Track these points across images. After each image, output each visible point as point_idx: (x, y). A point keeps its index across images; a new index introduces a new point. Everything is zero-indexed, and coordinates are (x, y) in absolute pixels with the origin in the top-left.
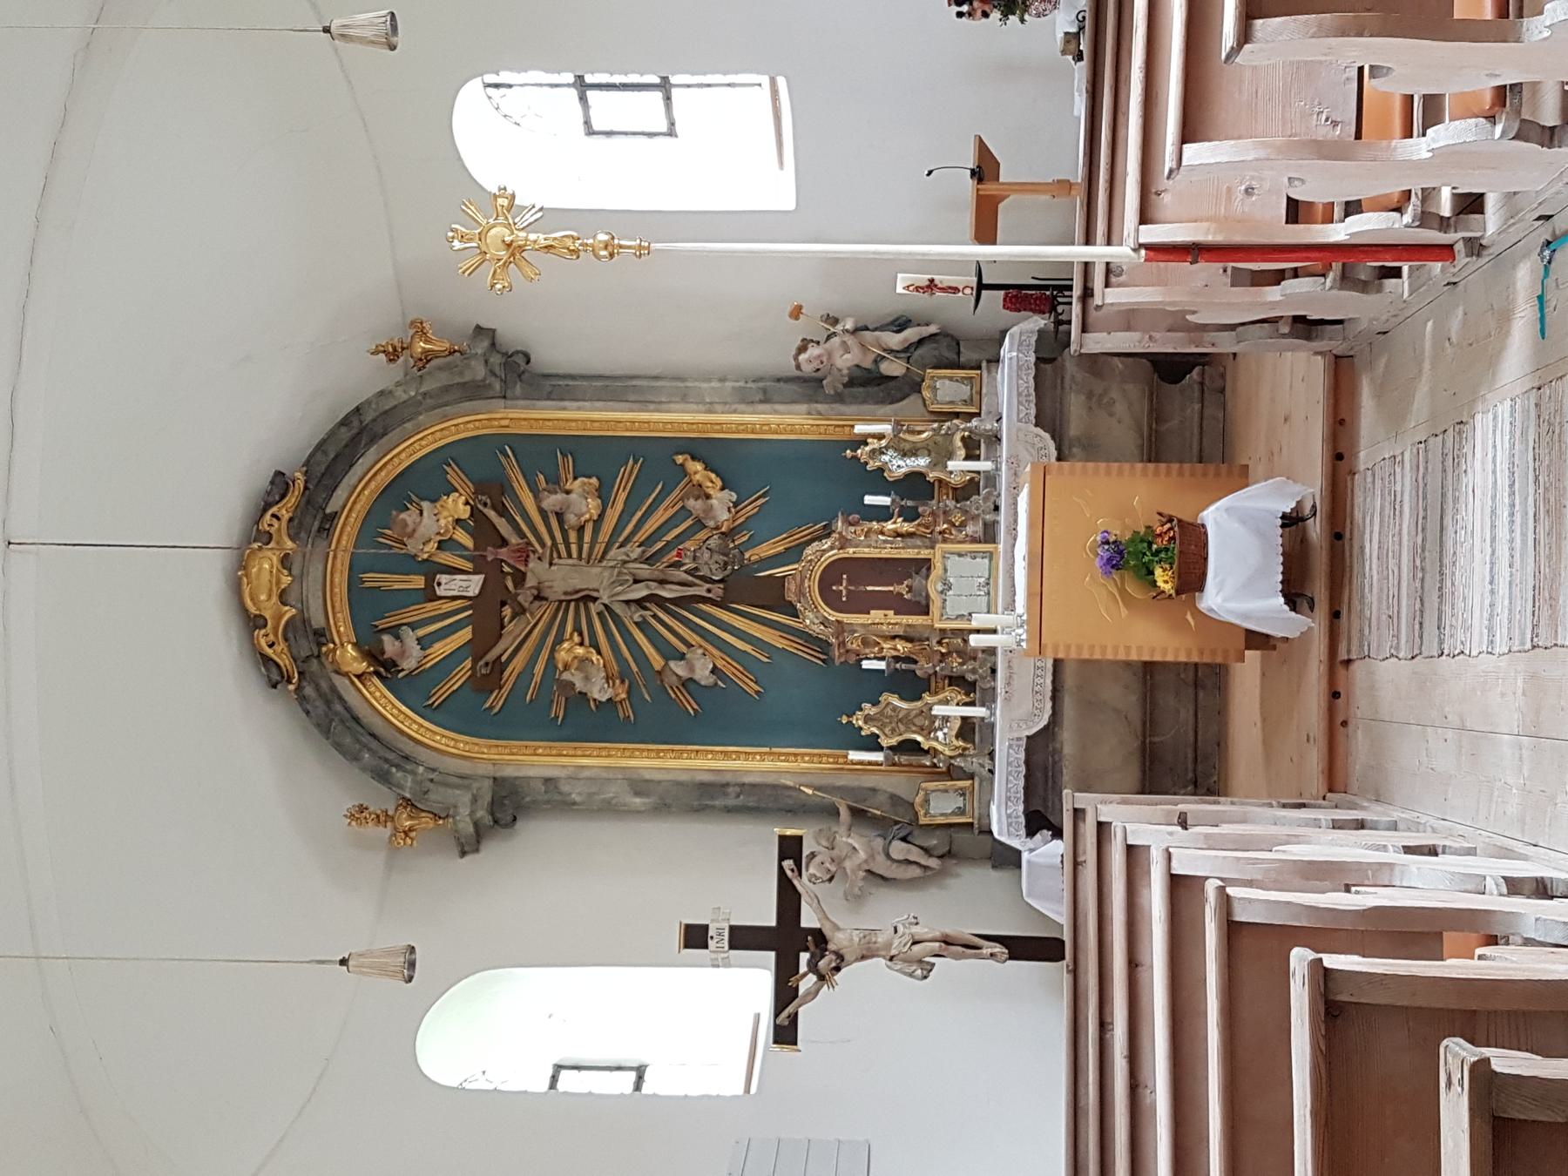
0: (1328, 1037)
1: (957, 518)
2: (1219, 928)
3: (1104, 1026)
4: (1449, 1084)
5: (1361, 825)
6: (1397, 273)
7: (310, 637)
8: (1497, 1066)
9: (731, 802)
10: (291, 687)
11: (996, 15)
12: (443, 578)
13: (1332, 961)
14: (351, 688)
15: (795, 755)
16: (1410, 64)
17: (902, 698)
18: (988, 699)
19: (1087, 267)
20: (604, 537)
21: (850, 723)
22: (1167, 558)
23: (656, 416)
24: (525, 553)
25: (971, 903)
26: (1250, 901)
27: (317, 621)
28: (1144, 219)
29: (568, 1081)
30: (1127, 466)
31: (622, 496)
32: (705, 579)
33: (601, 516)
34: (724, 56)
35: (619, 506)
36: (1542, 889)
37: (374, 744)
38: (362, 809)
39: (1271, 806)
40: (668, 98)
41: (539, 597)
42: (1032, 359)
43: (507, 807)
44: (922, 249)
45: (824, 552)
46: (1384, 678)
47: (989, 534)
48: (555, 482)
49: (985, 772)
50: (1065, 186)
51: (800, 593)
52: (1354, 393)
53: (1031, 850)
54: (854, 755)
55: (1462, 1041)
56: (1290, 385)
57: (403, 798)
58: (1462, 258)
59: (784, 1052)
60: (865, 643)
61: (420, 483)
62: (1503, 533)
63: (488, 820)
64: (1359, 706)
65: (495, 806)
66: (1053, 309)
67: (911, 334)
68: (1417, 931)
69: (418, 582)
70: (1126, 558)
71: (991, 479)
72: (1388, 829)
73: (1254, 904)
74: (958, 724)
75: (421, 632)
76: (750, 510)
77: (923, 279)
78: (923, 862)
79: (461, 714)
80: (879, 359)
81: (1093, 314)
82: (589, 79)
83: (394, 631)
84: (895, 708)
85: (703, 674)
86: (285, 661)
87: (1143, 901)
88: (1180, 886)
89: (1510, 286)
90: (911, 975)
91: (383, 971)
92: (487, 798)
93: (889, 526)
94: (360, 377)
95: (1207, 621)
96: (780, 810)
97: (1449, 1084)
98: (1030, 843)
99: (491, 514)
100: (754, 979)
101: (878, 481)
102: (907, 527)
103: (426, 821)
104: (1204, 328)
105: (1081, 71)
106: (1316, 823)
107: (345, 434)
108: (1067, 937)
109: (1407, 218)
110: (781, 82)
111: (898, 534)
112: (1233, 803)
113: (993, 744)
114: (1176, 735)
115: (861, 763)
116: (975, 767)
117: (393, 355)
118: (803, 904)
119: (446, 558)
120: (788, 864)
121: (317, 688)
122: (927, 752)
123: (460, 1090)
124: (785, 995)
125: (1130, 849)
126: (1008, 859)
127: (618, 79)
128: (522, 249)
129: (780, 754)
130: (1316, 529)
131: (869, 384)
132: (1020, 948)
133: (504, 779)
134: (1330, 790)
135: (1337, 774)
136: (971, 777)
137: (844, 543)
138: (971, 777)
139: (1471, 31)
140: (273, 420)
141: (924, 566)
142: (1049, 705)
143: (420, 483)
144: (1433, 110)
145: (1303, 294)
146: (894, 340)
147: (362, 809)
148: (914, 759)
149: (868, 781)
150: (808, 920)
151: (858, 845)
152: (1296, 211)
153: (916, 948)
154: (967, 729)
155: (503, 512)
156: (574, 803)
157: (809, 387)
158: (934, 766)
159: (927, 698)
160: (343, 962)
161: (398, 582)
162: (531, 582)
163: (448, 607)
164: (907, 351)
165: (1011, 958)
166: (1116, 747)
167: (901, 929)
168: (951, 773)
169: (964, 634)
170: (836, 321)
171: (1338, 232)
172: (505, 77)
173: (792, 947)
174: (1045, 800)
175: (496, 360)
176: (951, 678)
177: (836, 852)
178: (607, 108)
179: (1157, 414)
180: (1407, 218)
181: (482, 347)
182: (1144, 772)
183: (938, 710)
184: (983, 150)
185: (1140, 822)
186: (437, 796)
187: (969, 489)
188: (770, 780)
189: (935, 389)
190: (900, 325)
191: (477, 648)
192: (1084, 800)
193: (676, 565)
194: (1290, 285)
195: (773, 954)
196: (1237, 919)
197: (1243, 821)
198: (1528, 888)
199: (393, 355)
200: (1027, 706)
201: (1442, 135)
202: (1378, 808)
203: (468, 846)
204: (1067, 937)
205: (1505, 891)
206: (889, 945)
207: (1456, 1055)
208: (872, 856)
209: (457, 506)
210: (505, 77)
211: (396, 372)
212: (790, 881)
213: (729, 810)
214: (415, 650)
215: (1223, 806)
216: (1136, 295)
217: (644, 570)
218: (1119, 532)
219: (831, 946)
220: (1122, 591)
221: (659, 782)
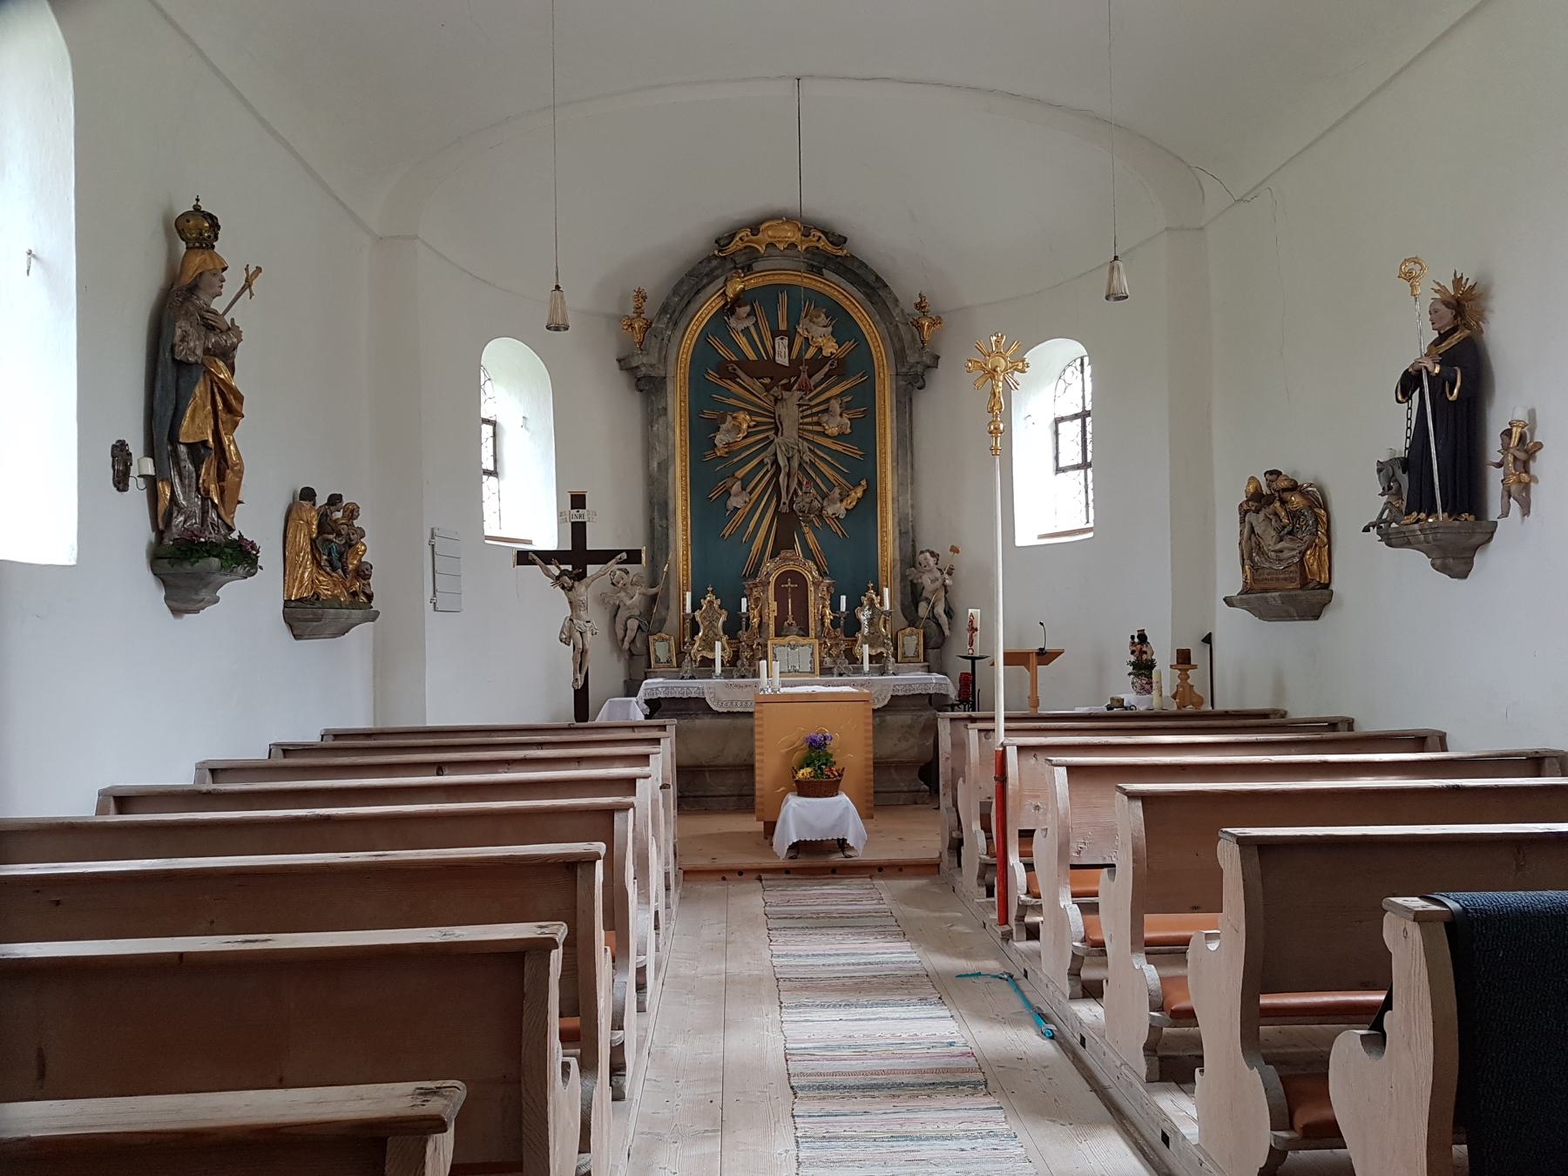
1: (834, 652)
3: (541, 745)
5: (667, 888)
6: (990, 894)
7: (747, 262)
11: (1133, 658)
12: (786, 341)
13: (599, 864)
16: (1116, 893)
18: (726, 674)
19: (992, 719)
20: (819, 439)
22: (818, 777)
23: (889, 467)
24: (805, 389)
25: (606, 669)
27: (757, 266)
28: (1021, 749)
29: (487, 430)
30: (871, 749)
31: (840, 448)
32: (792, 502)
33: (828, 436)
34: (1104, 500)
35: (834, 447)
36: (641, 987)
38: (644, 298)
40: (1077, 467)
41: (776, 400)
42: (931, 691)
43: (648, 385)
44: (998, 625)
45: (810, 573)
46: (753, 900)
47: (825, 671)
48: (846, 407)
50: (1035, 703)
51: (785, 559)
52: (918, 876)
54: (688, 595)
56: (920, 839)
58: (1000, 930)
59: (512, 558)
60: (757, 599)
61: (843, 326)
62: (842, 960)
63: (640, 374)
64: (733, 887)
65: (649, 379)
66: (961, 702)
67: (944, 619)
69: (783, 326)
70: (816, 751)
71: (859, 671)
73: (625, 825)
75: (752, 329)
76: (834, 527)
77: (977, 625)
80: (928, 601)
81: (962, 724)
82: (1088, 420)
83: (752, 313)
85: (734, 502)
86: (732, 247)
88: (629, 784)
89: (986, 957)
91: (553, 311)
93: (828, 611)
94: (906, 287)
95: (781, 799)
98: (641, 702)
99: (826, 369)
100: (547, 536)
101: (854, 604)
102: (827, 622)
103: (638, 337)
104: (955, 789)
105: (1102, 709)
106: (667, 863)
107: (871, 279)
109: (1023, 897)
110: (1091, 535)
111: (823, 617)
114: (714, 784)
117: (920, 306)
118: (599, 567)
119: (798, 341)
120: (624, 556)
121: (716, 268)
124: (546, 557)
125: (646, 757)
126: (631, 689)
127: (1089, 436)
128: (993, 378)
130: (837, 858)
131: (912, 595)
135: (692, 876)
136: (679, 666)
137: (816, 584)
138: (679, 666)
139: (1137, 925)
140: (879, 233)
141: (805, 632)
143: (843, 326)
144: (1089, 909)
145: (977, 842)
146: (940, 609)
147: (644, 298)
150: (592, 569)
151: (634, 600)
152: (1026, 835)
155: (828, 376)
157: (910, 560)
159: (725, 638)
160: (557, 287)
161: (782, 314)
162: (786, 394)
163: (769, 345)
164: (933, 617)
166: (703, 751)
168: (681, 654)
169: (766, 658)
170: (950, 574)
171: (1014, 860)
172: (1088, 370)
173: (574, 560)
175: (919, 369)
178: (1071, 430)
179: (900, 766)
180: (1023, 897)
181: (927, 360)
183: (718, 645)
184: (1057, 654)
185: (660, 765)
186: (654, 344)
187: (853, 659)
188: (672, 545)
189: (911, 635)
190: (949, 612)
191: (743, 363)
192: (671, 731)
193: (800, 483)
194: (981, 836)
199: (920, 306)
200: (724, 698)
201: (1074, 912)
206: (579, 618)
209: (830, 348)
210: (1088, 370)
211: (910, 308)
213: (652, 521)
214: (741, 326)
215: (673, 812)
216: (969, 749)
217: (795, 464)
218: (832, 746)
220: (795, 750)
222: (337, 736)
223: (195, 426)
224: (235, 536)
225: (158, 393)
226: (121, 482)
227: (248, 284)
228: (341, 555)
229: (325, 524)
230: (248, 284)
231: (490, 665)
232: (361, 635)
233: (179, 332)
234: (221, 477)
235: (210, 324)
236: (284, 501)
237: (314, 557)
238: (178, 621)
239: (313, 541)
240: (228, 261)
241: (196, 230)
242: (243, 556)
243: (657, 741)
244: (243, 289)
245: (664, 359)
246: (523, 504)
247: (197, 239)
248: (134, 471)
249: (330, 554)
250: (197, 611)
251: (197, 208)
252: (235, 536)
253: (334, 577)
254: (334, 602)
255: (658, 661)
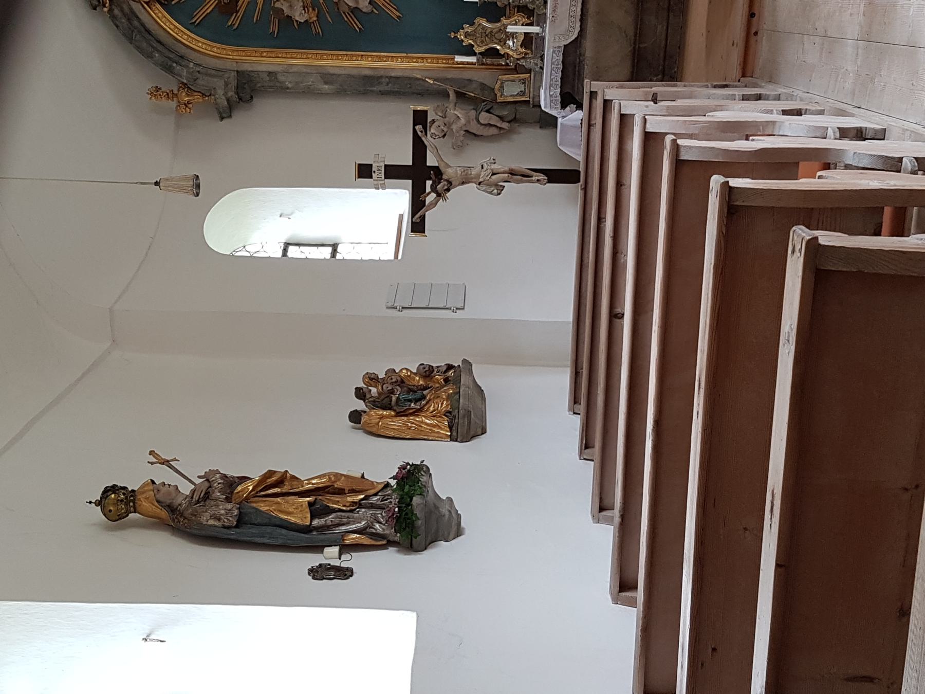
0: (727, 226)
2: (671, 164)
3: (600, 219)
4: (793, 252)
5: (759, 97)
8: (823, 241)
9: (383, 88)
10: (106, 9)
13: (735, 182)
14: (143, 11)
15: (423, 58)
17: (488, 21)
18: (541, 20)
21: (456, 37)
25: (526, 149)
26: (690, 147)
29: (293, 252)
36: (860, 134)
37: (160, 48)
38: (158, 89)
39: (707, 87)
43: (245, 91)
49: (537, 69)
53: (563, 117)
54: (459, 59)
55: (803, 227)
57: (183, 83)
63: (235, 98)
65: (239, 88)
68: (784, 162)
72: (775, 100)
74: (522, 37)
78: (499, 125)
79: (216, 29)
84: (484, 28)
87: (628, 147)
88: (651, 140)
90: (491, 193)
91: (181, 189)
92: (234, 83)
96: (413, 93)
97: (793, 252)
98: (563, 113)
100: (398, 198)
103: (198, 98)
106: (733, 97)
108: (582, 169)
112: (685, 86)
113: (543, 51)
115: (462, 63)
116: (532, 66)
120: (419, 128)
121: (122, 10)
122: (503, 56)
123: (232, 256)
124: (417, 205)
126: (549, 122)
129: (413, 58)
132: (554, 176)
133: (243, 72)
134: (743, 76)
135: (749, 66)
136: (529, 71)
138: (529, 71)
142: (578, 24)
147: (158, 89)
148: (495, 61)
149: (467, 75)
150: (431, 161)
151: (460, 115)
153: (494, 177)
154: (528, 41)
156: (288, 88)
158: (507, 65)
159: (504, 21)
160: (157, 184)
165: (549, 182)
166: (617, 51)
167: (485, 166)
168: (518, 69)
173: (421, 178)
174: (573, 87)
176: (518, 7)
177: (446, 120)
182: (633, 66)
183: (510, 29)
186: (202, 81)
188: (407, 74)
192: (596, 86)
195: (410, 181)
196: (682, 158)
197: (690, 97)
198: (853, 133)
202: (770, 86)
203: (225, 113)
204: (582, 169)
205: (838, 135)
206: (478, 176)
207: (799, 235)
208: (468, 122)
212: (420, 138)
213: (383, 93)
215: (679, 88)
219: (444, 177)
221: (340, 75)
222: (575, 400)
223: (296, 512)
224: (393, 483)
225: (266, 541)
226: (345, 573)
227: (166, 462)
228: (410, 390)
229: (382, 403)
230: (166, 462)
231: (518, 264)
232: (483, 376)
233: (211, 522)
234: (341, 492)
235: (204, 497)
236: (361, 436)
237: (412, 414)
238: (467, 532)
239: (398, 414)
240: (147, 479)
241: (118, 504)
242: (412, 477)
243: (607, 103)
244: (171, 467)
245: (219, 72)
246: (367, 221)
247: (127, 504)
248: (336, 563)
249: (410, 401)
250: (459, 516)
251: (98, 503)
252: (393, 483)
253: (429, 397)
254: (454, 399)
255: (522, 93)
